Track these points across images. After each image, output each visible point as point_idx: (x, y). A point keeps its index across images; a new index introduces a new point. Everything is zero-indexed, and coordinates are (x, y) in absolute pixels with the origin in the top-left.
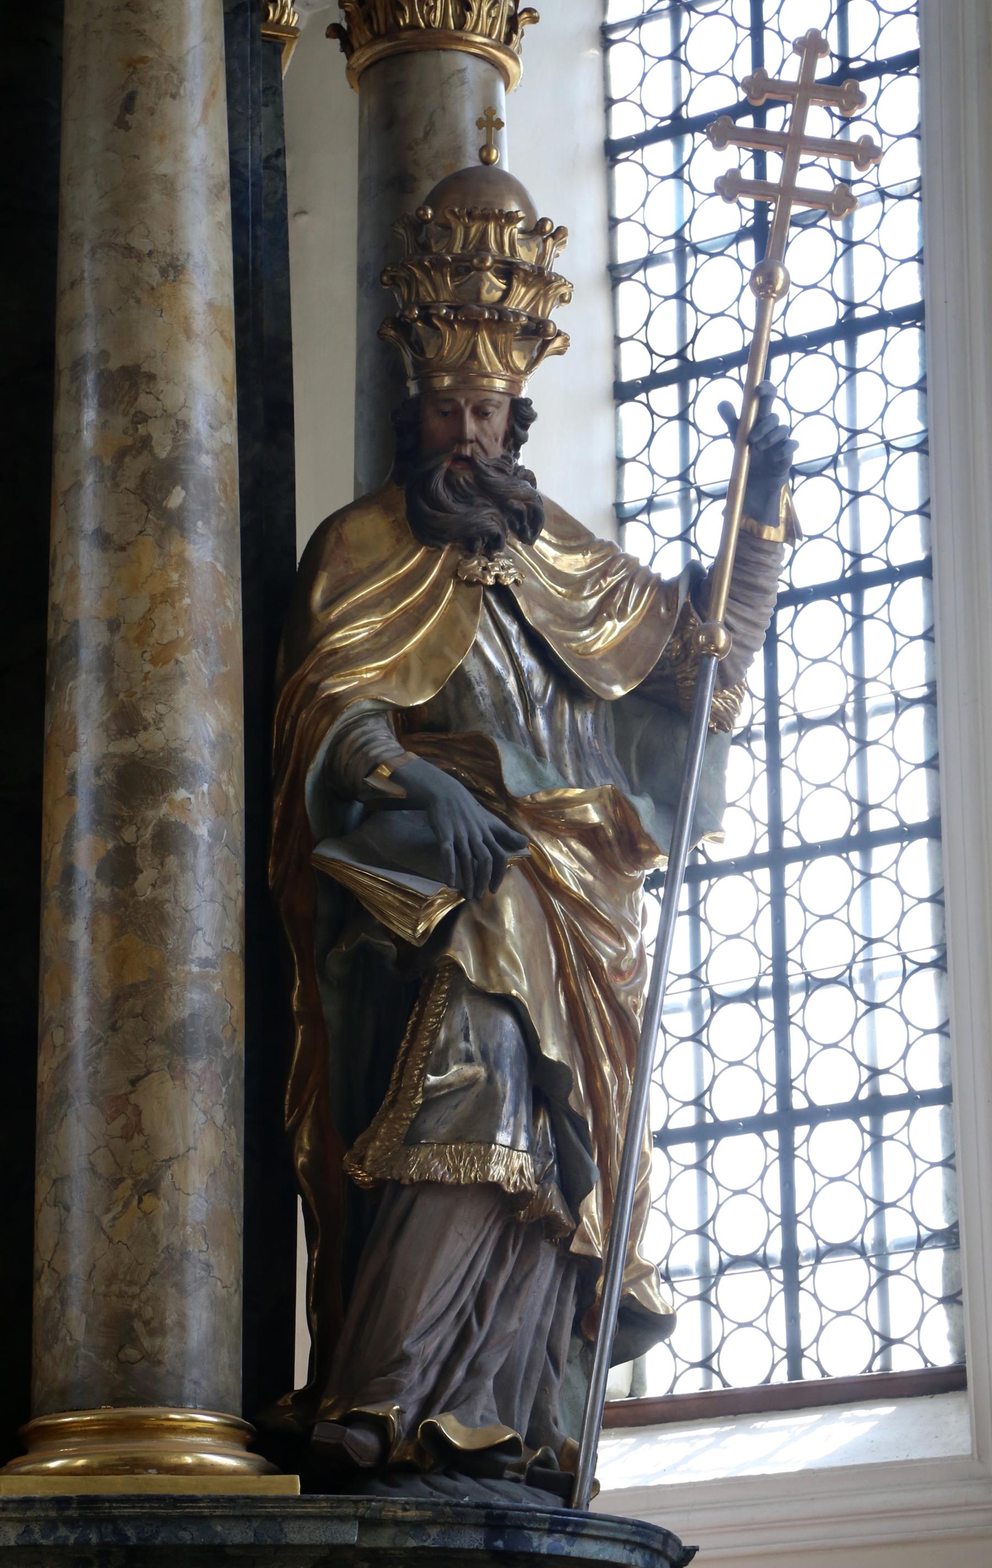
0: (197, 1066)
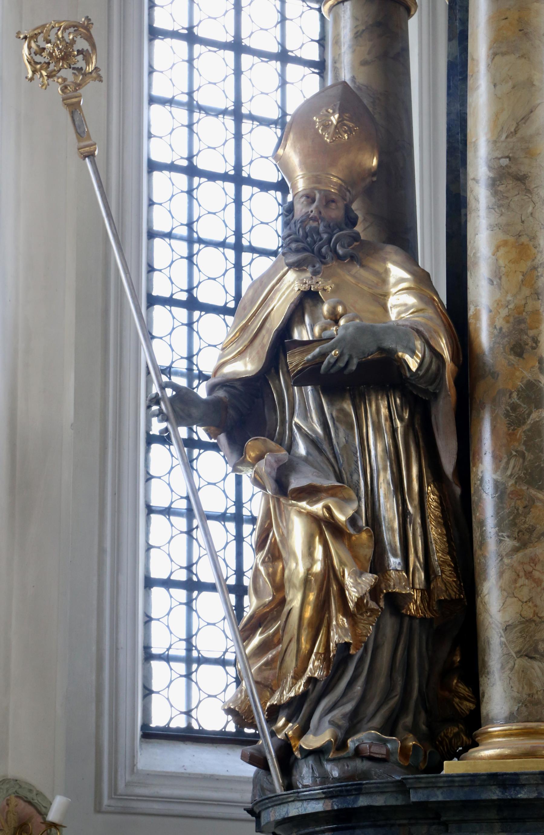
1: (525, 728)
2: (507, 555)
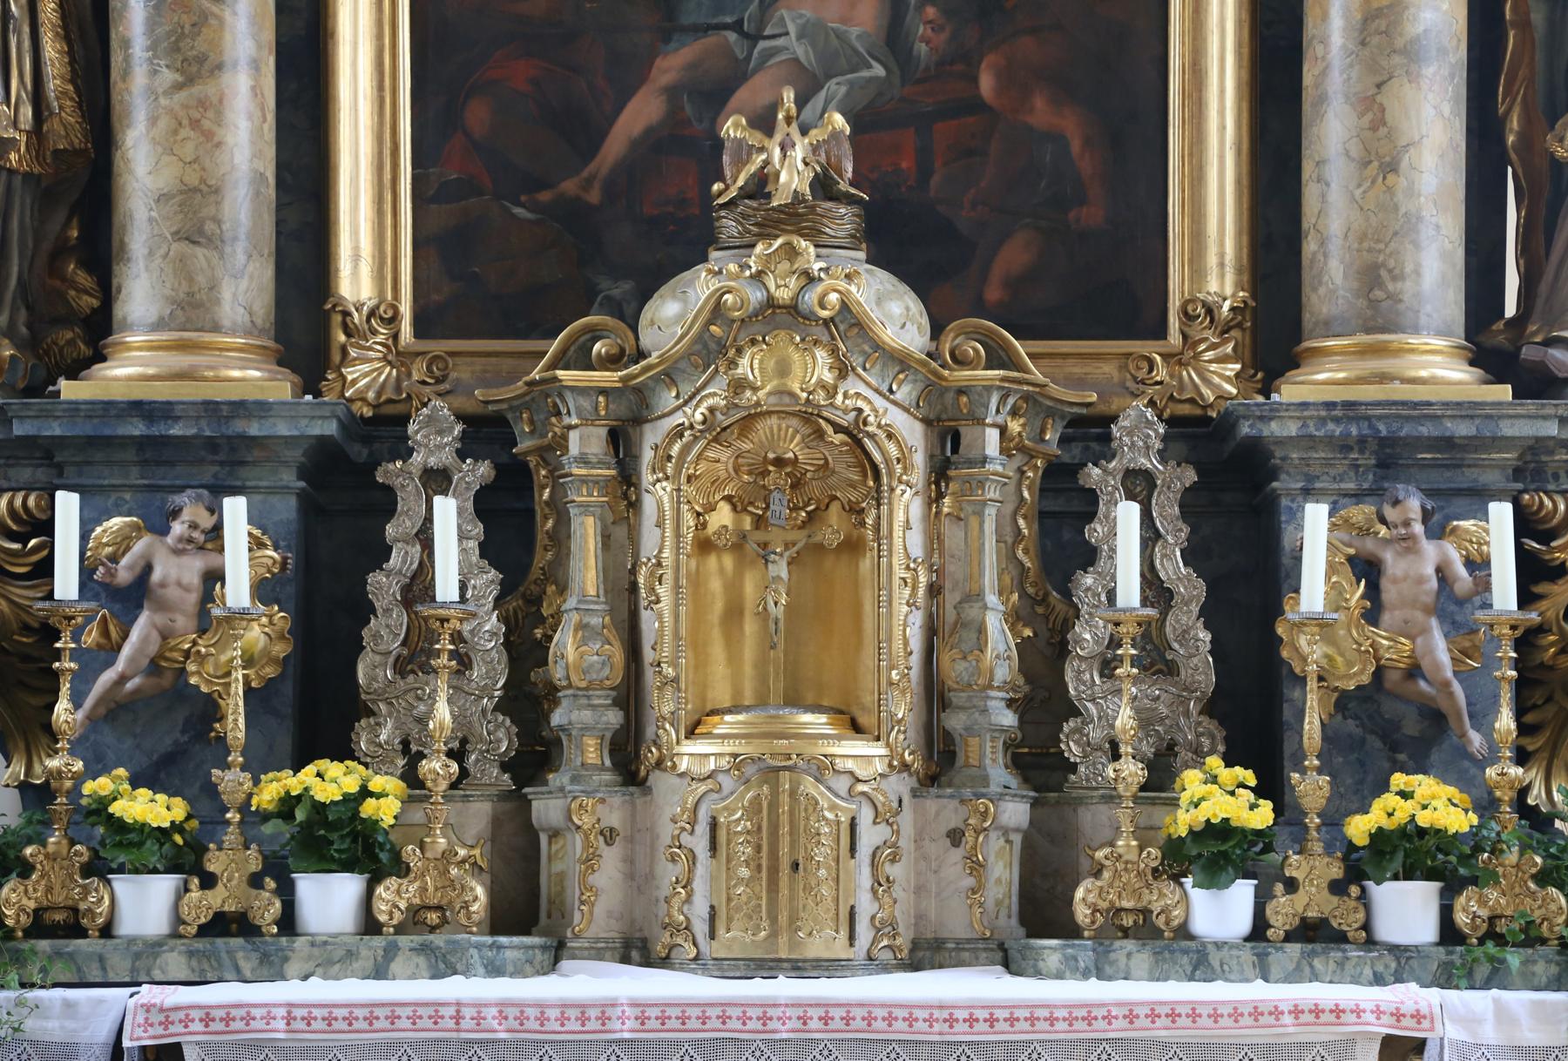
0: (1429, 71)
1: (181, 339)
2: (165, 93)
